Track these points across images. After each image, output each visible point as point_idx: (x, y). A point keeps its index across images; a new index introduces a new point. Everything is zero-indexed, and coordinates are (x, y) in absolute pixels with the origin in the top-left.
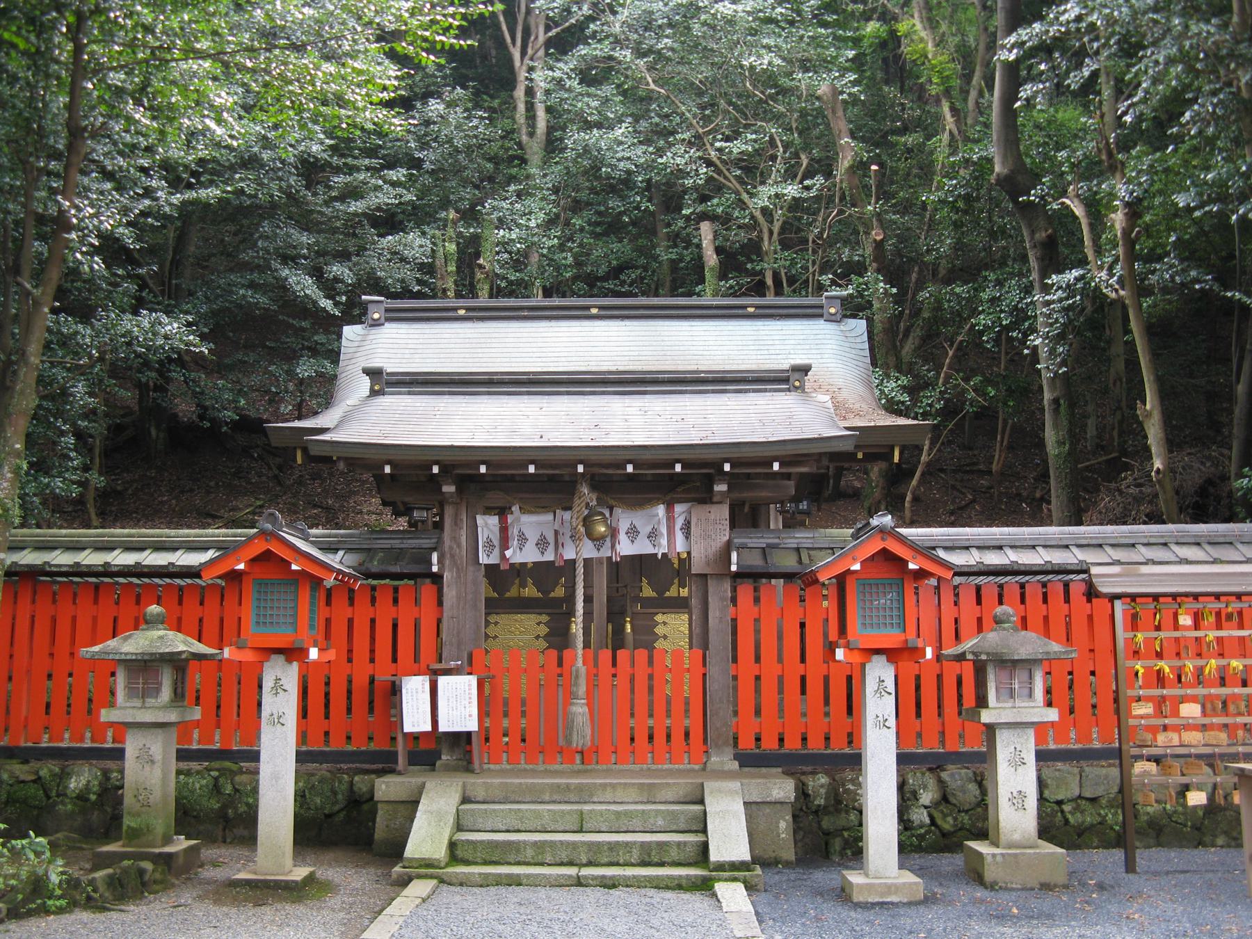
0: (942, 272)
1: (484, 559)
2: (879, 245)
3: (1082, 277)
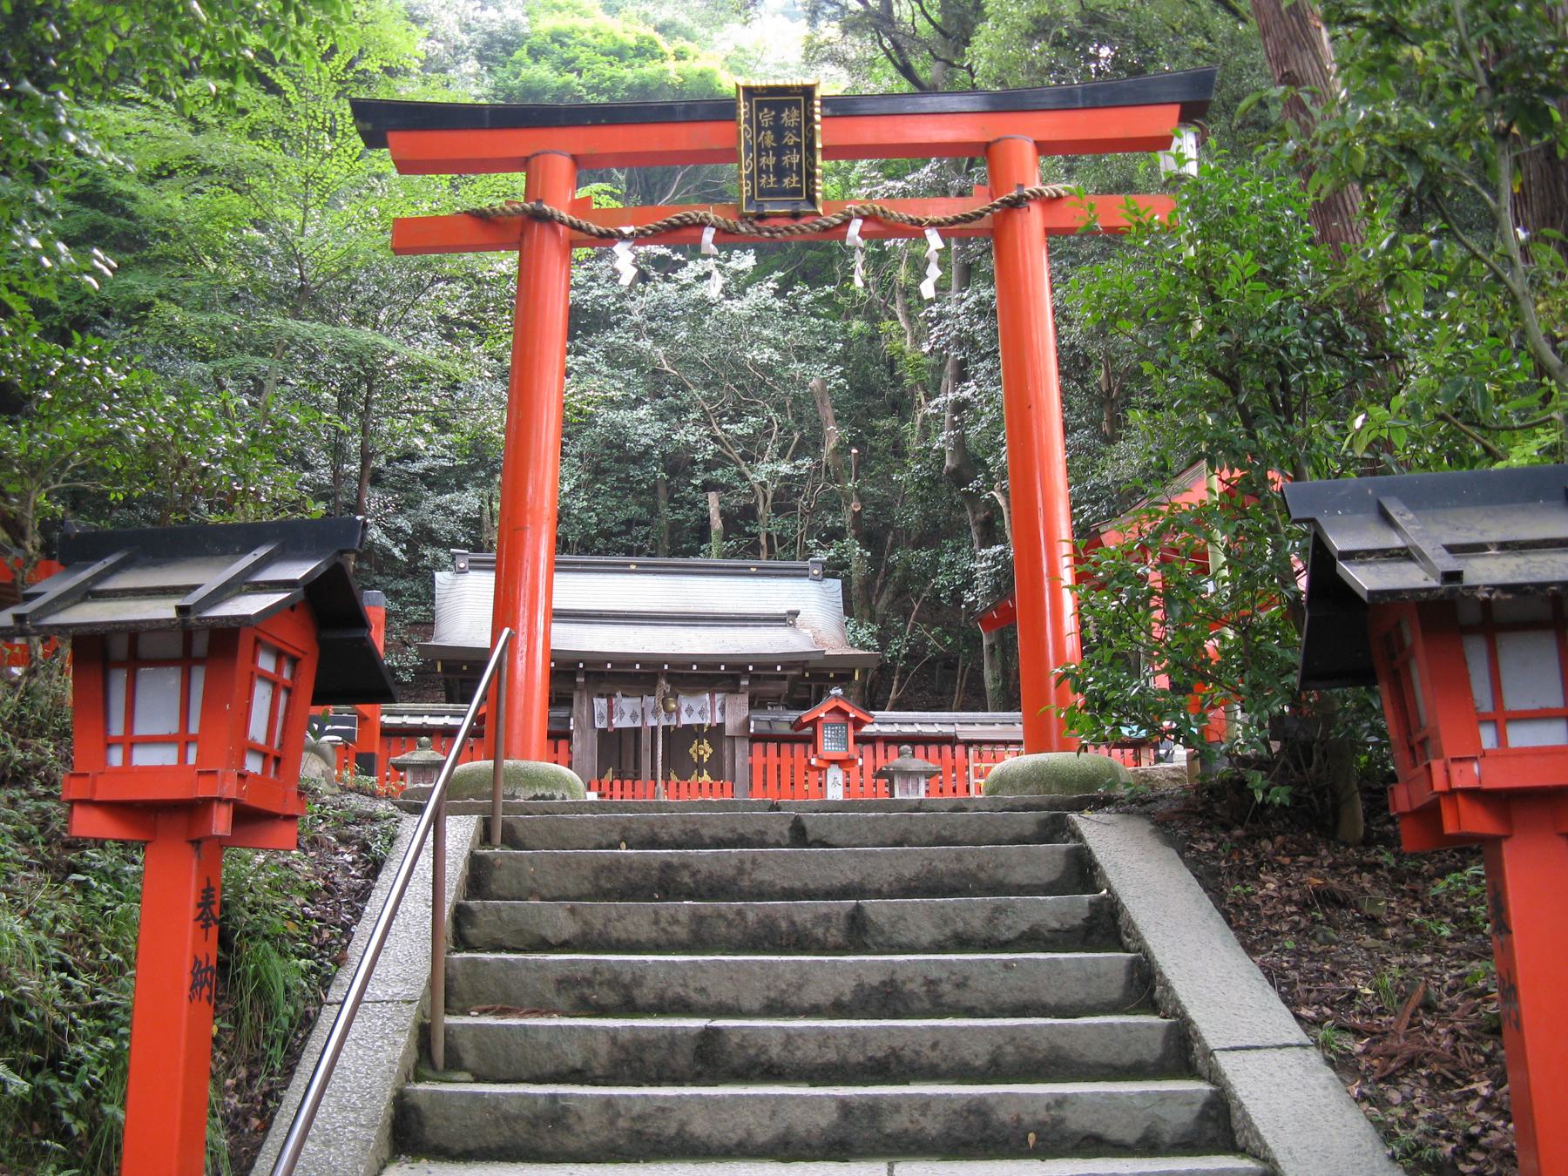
0: (914, 537)
1: (598, 726)
2: (857, 515)
3: (1002, 552)
